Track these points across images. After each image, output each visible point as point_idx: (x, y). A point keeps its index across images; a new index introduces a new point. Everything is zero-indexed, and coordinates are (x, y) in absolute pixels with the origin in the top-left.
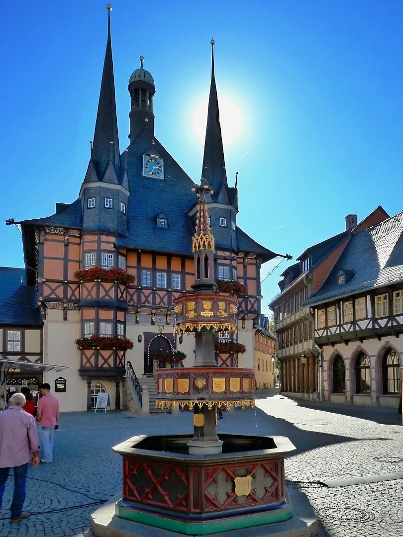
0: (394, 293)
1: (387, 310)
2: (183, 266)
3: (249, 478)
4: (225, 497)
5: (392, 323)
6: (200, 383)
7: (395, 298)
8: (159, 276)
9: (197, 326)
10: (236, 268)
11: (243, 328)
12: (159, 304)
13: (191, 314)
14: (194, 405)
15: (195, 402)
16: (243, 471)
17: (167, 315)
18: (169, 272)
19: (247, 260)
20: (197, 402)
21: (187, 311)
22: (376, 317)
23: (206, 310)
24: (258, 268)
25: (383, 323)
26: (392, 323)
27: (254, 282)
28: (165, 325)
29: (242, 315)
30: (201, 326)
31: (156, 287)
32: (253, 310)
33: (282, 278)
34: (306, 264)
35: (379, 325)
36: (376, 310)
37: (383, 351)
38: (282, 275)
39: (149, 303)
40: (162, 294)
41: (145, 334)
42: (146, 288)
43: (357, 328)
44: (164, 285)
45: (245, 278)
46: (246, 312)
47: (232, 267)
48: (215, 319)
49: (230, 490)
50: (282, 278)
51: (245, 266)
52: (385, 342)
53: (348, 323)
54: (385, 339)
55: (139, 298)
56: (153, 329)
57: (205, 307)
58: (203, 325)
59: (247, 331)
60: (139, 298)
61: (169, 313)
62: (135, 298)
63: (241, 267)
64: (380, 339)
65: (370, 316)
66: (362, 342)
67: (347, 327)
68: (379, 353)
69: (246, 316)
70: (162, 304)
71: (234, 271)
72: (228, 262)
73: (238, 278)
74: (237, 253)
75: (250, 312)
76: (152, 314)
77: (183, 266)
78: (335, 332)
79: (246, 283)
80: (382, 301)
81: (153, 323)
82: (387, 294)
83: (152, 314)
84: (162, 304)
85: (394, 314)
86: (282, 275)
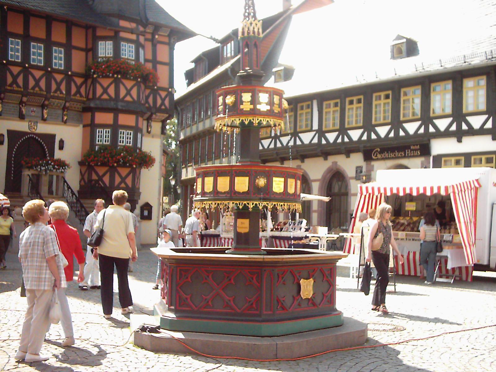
0: (348, 100)
1: (338, 121)
2: (69, 36)
3: (311, 281)
4: (291, 298)
5: (343, 139)
6: (262, 182)
7: (348, 106)
8: (34, 48)
9: (253, 120)
10: (143, 47)
11: (149, 132)
12: (33, 88)
13: (246, 107)
14: (254, 205)
15: (255, 203)
16: (305, 273)
17: (43, 106)
18: (49, 44)
19: (157, 37)
20: (257, 203)
21: (242, 103)
22: (324, 129)
24: (172, 49)
25: (331, 137)
26: (343, 139)
27: (166, 68)
28: (39, 120)
29: (148, 114)
30: (258, 120)
31: (29, 64)
32: (163, 107)
33: (193, 66)
34: (229, 49)
35: (326, 139)
36: (298, 122)
37: (328, 175)
38: (192, 62)
39: (18, 86)
40: (59, 77)
41: (9, 132)
42: (59, 72)
43: (299, 142)
44: (40, 61)
45: (155, 62)
46: (153, 111)
47: (138, 45)
48: (270, 114)
49: (295, 293)
50: (193, 66)
51: (154, 46)
52: (333, 163)
53: (287, 135)
54: (332, 159)
55: (26, 82)
56: (22, 126)
57: (244, 99)
59: (153, 137)
60: (26, 82)
61: (46, 103)
62: (20, 80)
63: (149, 45)
64: (326, 159)
65: (316, 126)
66: (303, 161)
67: (285, 140)
68: (324, 177)
69: (154, 116)
70: (37, 89)
71: (141, 52)
72: (134, 37)
73: (146, 60)
74: (145, 26)
75: (159, 110)
76: (21, 103)
77: (69, 36)
78: (269, 146)
79: (155, 68)
80: (332, 109)
81: (22, 117)
82: (338, 101)
83: (21, 103)
84: (37, 89)
85: (346, 126)
86: (192, 62)
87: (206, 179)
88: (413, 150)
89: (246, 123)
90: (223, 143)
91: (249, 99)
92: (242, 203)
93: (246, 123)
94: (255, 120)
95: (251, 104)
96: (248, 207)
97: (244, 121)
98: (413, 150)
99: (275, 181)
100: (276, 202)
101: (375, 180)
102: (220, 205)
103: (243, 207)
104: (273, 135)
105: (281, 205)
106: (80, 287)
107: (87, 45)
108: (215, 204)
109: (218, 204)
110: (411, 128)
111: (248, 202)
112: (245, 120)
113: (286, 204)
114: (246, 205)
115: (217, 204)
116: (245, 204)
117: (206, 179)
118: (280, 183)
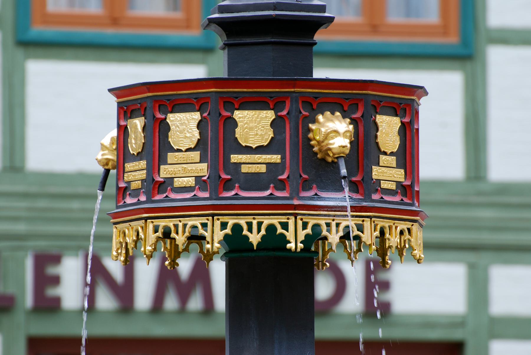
9: (204, 225)
23: (385, 153)
58: (231, 222)
89: (255, 238)
90: (144, 203)
93: (255, 238)
94: (291, 227)
95: (201, 162)
97: (245, 232)
101: (421, 104)
102: (173, 235)
103: (263, 237)
104: (320, 242)
111: (284, 219)
112: (250, 230)
113: (367, 224)
114: (276, 229)
115: (161, 230)
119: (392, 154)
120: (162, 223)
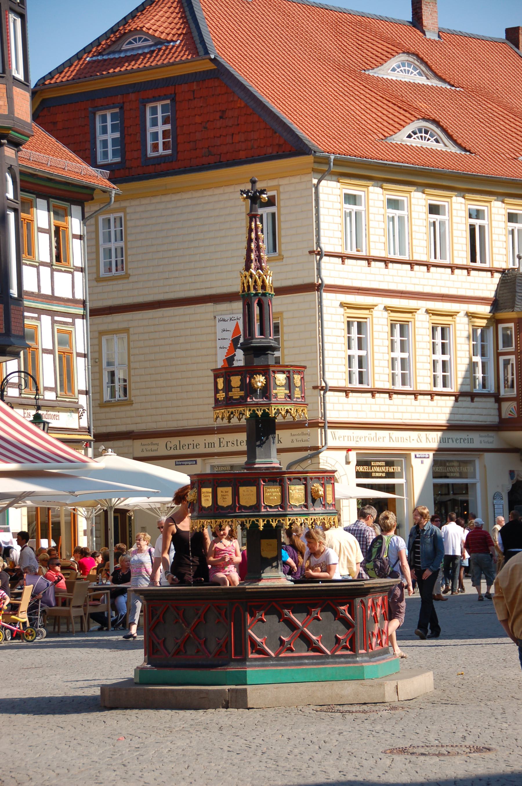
9: (268, 409)
14: (265, 522)
23: (280, 386)
87: (220, 490)
88: (383, 472)
91: (239, 383)
92: (250, 521)
95: (240, 391)
96: (257, 524)
98: (383, 472)
99: (204, 493)
100: (220, 519)
105: (228, 522)
106: (280, 639)
107: (320, 297)
108: (311, 519)
109: (314, 519)
110: (447, 464)
112: (272, 522)
116: (253, 522)
117: (220, 490)
118: (208, 494)
119: (237, 387)
120: (230, 410)
